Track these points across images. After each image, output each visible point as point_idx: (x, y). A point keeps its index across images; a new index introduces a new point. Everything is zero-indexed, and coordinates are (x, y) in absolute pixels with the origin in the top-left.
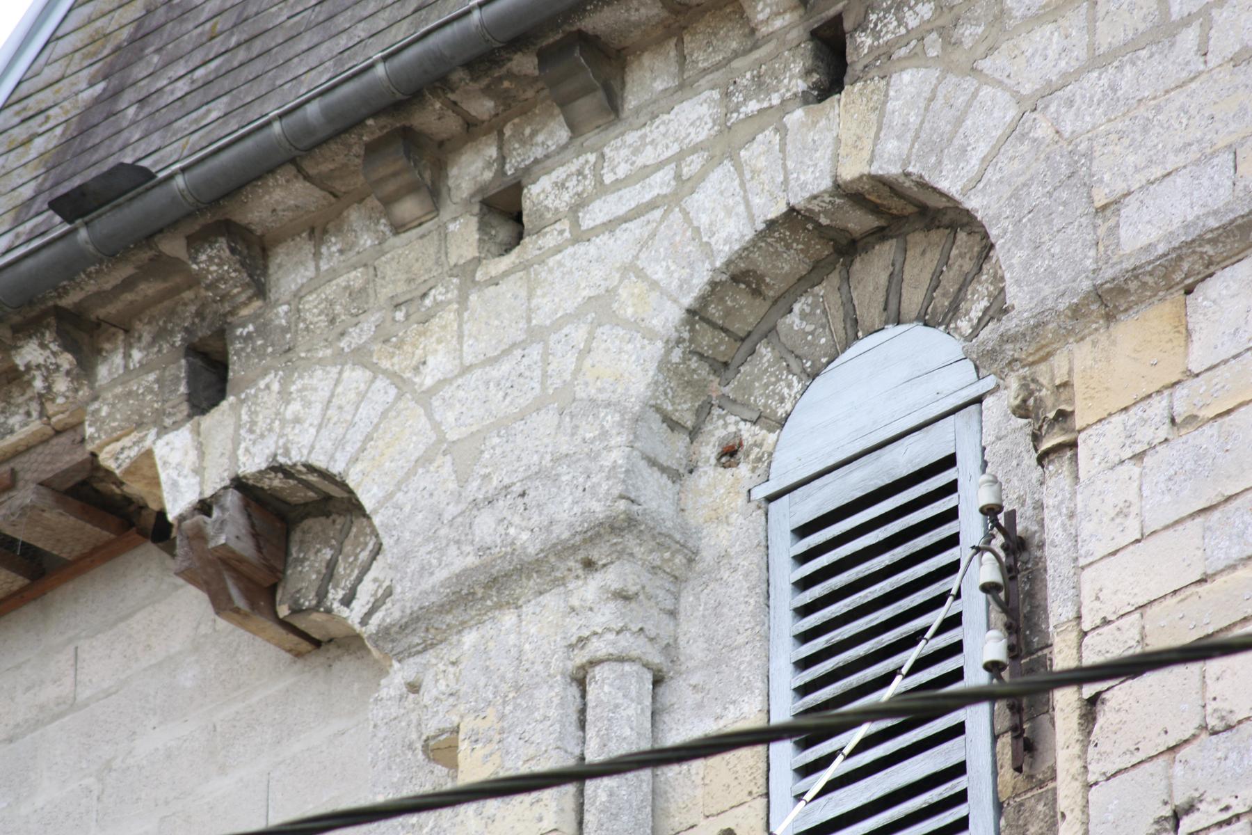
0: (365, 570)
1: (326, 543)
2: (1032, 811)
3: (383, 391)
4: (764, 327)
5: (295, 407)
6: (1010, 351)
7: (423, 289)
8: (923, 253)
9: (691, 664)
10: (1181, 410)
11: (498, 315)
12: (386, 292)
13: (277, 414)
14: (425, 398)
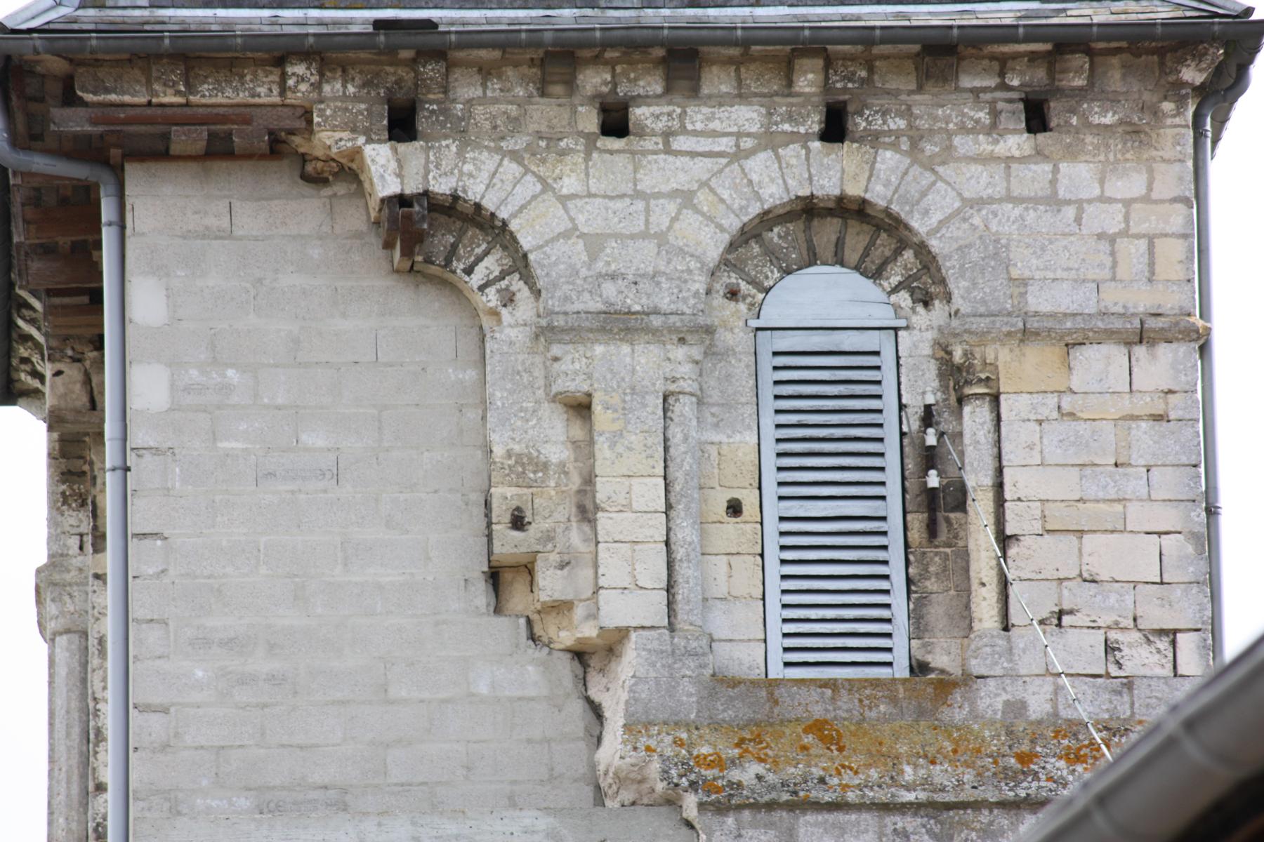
0: (479, 259)
1: (450, 232)
2: (932, 559)
3: (530, 186)
4: (755, 232)
5: (468, 167)
6: (966, 337)
7: (560, 136)
8: (858, 234)
9: (711, 401)
10: (1066, 407)
11: (613, 173)
12: (533, 127)
13: (456, 165)
14: (564, 200)
